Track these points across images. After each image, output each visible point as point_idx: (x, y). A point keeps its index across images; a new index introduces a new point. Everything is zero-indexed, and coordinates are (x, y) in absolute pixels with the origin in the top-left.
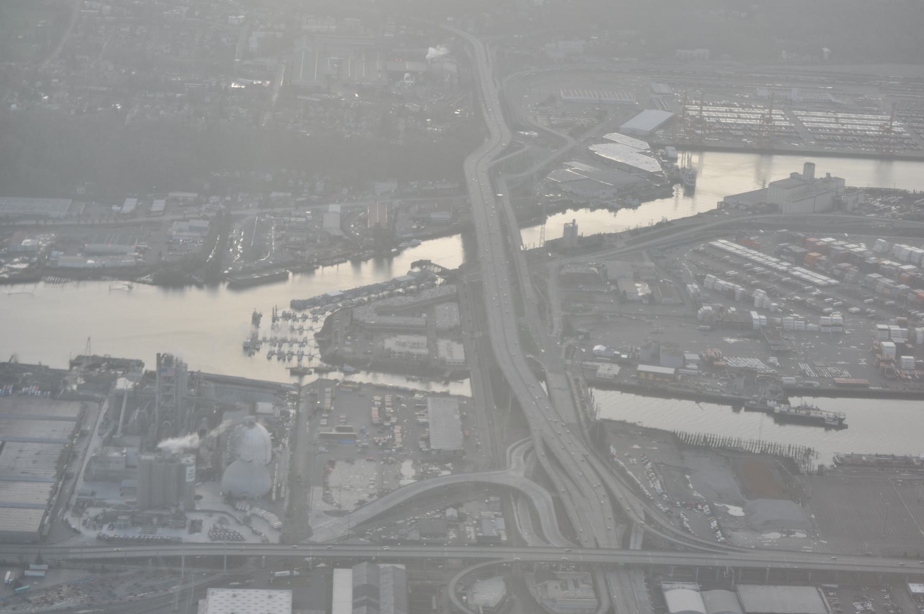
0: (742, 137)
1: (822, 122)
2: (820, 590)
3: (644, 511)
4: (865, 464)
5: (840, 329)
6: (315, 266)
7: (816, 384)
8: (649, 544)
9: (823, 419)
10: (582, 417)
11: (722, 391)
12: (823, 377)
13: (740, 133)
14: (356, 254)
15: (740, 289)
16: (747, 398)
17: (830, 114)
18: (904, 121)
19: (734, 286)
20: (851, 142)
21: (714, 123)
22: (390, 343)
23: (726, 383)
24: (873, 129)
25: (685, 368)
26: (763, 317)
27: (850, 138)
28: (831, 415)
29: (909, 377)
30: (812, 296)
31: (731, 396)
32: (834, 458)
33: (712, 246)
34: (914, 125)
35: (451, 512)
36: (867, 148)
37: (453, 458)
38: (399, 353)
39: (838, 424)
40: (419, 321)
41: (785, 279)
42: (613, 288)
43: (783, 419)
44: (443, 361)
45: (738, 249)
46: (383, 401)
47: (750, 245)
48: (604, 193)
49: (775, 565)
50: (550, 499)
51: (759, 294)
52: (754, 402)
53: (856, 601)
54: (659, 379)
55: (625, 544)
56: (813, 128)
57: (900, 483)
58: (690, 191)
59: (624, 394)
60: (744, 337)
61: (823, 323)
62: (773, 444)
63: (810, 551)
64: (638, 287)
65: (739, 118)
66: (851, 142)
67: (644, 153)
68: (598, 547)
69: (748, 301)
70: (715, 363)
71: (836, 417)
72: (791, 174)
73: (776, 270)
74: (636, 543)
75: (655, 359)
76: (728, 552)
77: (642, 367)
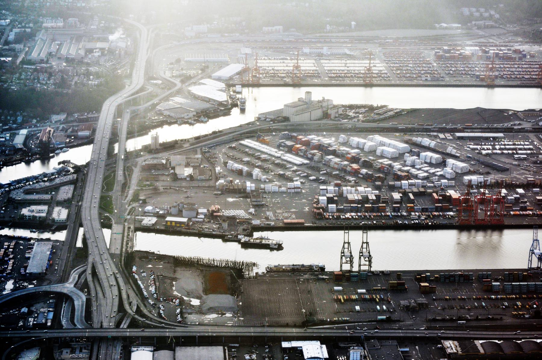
0: (285, 77)
1: (336, 66)
2: (226, 348)
3: (138, 306)
4: (284, 271)
5: (299, 190)
7: (273, 223)
8: (134, 324)
9: (269, 245)
10: (124, 250)
11: (214, 231)
12: (278, 219)
14: (27, 159)
15: (245, 169)
16: (227, 234)
17: (343, 61)
18: (387, 63)
19: (242, 168)
20: (349, 77)
21: (270, 70)
22: (25, 211)
24: (535, 70)
26: (253, 185)
27: (349, 75)
28: (274, 242)
29: (331, 217)
30: (291, 171)
31: (218, 233)
33: (241, 144)
34: (392, 65)
35: (24, 310)
36: (358, 80)
37: (40, 278)
38: (29, 216)
40: (47, 197)
41: (277, 161)
42: (172, 171)
43: (246, 246)
44: (53, 220)
45: (255, 145)
46: (9, 246)
47: (263, 142)
48: (188, 115)
49: (202, 334)
50: (85, 300)
51: (256, 172)
52: (231, 236)
53: (247, 354)
54: (178, 225)
55: (118, 325)
56: (328, 70)
57: (301, 281)
58: (243, 111)
59: (157, 235)
61: (289, 187)
62: (241, 262)
63: (231, 325)
64: (186, 171)
65: (287, 66)
66: (349, 77)
67: (221, 90)
68: (101, 327)
69: (249, 175)
70: (215, 214)
72: (299, 99)
75: (180, 214)
76: (176, 328)
77: (169, 219)
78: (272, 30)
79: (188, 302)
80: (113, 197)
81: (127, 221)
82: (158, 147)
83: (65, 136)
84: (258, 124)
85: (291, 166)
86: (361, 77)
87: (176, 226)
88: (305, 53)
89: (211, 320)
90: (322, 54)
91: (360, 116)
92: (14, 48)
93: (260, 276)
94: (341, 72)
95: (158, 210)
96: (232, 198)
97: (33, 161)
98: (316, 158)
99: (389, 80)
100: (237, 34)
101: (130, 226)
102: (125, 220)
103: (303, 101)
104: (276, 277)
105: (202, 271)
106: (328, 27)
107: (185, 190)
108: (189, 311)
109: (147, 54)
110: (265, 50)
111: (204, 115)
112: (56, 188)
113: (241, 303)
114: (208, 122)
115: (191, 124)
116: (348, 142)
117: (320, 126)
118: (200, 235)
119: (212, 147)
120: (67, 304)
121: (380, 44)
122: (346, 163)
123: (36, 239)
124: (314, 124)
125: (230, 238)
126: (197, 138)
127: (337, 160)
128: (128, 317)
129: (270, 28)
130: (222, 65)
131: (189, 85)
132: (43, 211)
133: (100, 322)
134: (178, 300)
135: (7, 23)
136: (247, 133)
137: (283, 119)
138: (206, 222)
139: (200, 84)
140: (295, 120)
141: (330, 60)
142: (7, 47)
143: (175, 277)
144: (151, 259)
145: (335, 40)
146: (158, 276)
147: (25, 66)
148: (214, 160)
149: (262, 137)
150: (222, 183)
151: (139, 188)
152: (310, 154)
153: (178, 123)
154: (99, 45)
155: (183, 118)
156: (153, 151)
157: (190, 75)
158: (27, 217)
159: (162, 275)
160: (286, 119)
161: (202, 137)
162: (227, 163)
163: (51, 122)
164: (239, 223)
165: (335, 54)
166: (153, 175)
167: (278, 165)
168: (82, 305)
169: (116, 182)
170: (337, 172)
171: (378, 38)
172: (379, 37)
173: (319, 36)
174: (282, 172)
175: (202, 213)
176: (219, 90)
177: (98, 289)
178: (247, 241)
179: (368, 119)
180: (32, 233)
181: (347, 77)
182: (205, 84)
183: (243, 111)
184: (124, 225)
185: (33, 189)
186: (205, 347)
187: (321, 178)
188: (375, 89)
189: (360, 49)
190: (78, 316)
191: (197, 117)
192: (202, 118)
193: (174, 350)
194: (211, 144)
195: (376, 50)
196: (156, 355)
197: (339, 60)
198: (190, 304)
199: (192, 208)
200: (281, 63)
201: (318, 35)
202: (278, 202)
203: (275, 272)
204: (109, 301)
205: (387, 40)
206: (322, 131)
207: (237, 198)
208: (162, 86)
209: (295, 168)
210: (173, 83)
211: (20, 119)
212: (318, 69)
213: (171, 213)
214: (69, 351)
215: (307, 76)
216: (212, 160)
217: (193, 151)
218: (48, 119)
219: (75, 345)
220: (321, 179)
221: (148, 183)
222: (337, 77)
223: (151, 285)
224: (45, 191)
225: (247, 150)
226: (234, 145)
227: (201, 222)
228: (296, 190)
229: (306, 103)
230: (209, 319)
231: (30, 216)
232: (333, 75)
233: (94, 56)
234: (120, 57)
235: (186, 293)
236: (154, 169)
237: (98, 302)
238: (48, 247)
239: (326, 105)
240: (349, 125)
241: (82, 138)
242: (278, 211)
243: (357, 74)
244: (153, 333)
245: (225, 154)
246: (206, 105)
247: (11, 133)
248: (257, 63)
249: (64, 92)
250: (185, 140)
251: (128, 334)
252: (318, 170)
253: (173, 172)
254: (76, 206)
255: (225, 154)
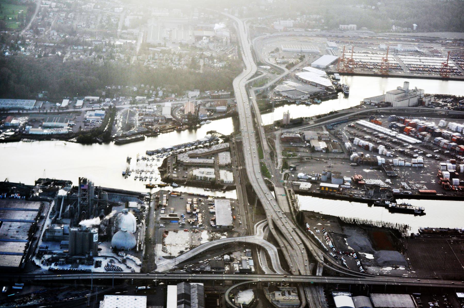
1: (413, 61)
5: (422, 165)
6: (158, 133)
7: (410, 192)
8: (326, 273)
10: (292, 209)
11: (362, 196)
13: (372, 67)
14: (179, 128)
15: (371, 145)
16: (375, 199)
17: (417, 57)
20: (427, 71)
23: (364, 192)
25: (344, 185)
27: (427, 69)
28: (417, 208)
29: (457, 189)
32: (419, 230)
33: (357, 124)
35: (226, 257)
37: (228, 230)
38: (200, 177)
39: (421, 213)
40: (211, 161)
42: (308, 144)
43: (393, 210)
44: (222, 181)
48: (303, 97)
49: (389, 283)
51: (381, 148)
52: (379, 202)
54: (331, 190)
58: (346, 95)
59: (313, 197)
60: (373, 169)
61: (413, 162)
65: (371, 59)
66: (427, 71)
69: (376, 151)
71: (420, 209)
73: (389, 135)
74: (319, 273)
75: (329, 180)
77: (322, 184)
78: (347, 27)
79: (363, 256)
80: (266, 164)
81: (285, 185)
82: (289, 123)
83: (206, 110)
84: (365, 107)
85: (407, 144)
86: (437, 72)
87: (329, 191)
88: (382, 49)
89: (388, 272)
90: (397, 50)
91: (448, 104)
92: (132, 32)
93: (416, 236)
94: (419, 66)
95: (310, 177)
96: (367, 169)
97: (184, 130)
98: (427, 139)
99: (461, 75)
100: (319, 30)
101: (290, 189)
102: (284, 184)
103: (402, 90)
104: (430, 238)
105: (365, 230)
106: (394, 27)
107: (325, 161)
108: (367, 263)
109: (249, 43)
110: (348, 44)
111: (317, 98)
112: (215, 154)
113: (408, 259)
114: (321, 104)
115: (307, 105)
116: (446, 126)
117: (418, 112)
118: (351, 199)
119: (334, 125)
120: (260, 253)
121: (443, 44)
122: (453, 144)
123: (213, 197)
124: (412, 109)
125: (378, 203)
126: (319, 117)
127: (446, 141)
128: (320, 267)
129: (346, 26)
130: (316, 56)
131: (294, 71)
132: (211, 173)
133: (297, 270)
134: (355, 254)
135: (121, 11)
136: (360, 114)
137: (386, 104)
138: (353, 189)
139: (303, 71)
140: (398, 106)
141: (405, 55)
142: (124, 31)
143: (344, 234)
144: (319, 218)
145: (403, 39)
146: (329, 233)
147: (150, 49)
148: (340, 136)
149: (375, 119)
150: (356, 156)
151: (286, 157)
152: (421, 135)
153: (297, 103)
154: (206, 33)
155: (300, 99)
156: (285, 126)
157: (292, 63)
158: (199, 178)
159: (333, 232)
160: (389, 104)
161: (323, 117)
162: (354, 139)
163: (188, 97)
164: (382, 191)
165: (407, 51)
166: (293, 147)
167: (395, 143)
168: (276, 255)
169: (264, 152)
170: (448, 151)
171: (438, 38)
172: (439, 38)
173: (389, 35)
174: (401, 149)
175: (348, 181)
176: (322, 77)
177: (285, 241)
178: (394, 207)
179: (456, 108)
180: (206, 192)
181: (425, 71)
182: (309, 71)
183: (346, 95)
184: (284, 188)
185: (195, 154)
186: (394, 295)
187: (436, 155)
188: (450, 82)
189: (427, 47)
190: (274, 263)
191: (311, 99)
192: (316, 100)
193: (369, 296)
194: (336, 122)
195: (442, 49)
196: (356, 300)
197: (412, 56)
198: (366, 258)
199: (339, 176)
200: (365, 56)
201: (388, 34)
202: (407, 174)
203: (427, 233)
204: (299, 252)
205: (447, 41)
206: (423, 115)
207: (371, 169)
208: (271, 71)
209: (411, 146)
210: (281, 69)
211: (161, 93)
212: (398, 63)
213: (321, 179)
214: (280, 293)
215: (391, 68)
216: (339, 136)
217: (319, 128)
218: (184, 94)
219: (283, 288)
220: (436, 157)
221: (291, 153)
222: (416, 70)
223: (327, 240)
224: (207, 156)
225: (365, 129)
226: (352, 124)
227: (349, 188)
228: (419, 165)
229: (405, 92)
230: (387, 271)
231: (202, 177)
232: (413, 69)
233: (203, 42)
234: (227, 44)
235: (359, 248)
236: (293, 142)
237: (289, 253)
238: (227, 205)
239: (419, 94)
240: (443, 112)
241: (220, 112)
242: (411, 182)
243: (433, 68)
244: (352, 281)
245: (346, 131)
246: (317, 89)
247: (157, 105)
248: (344, 55)
249: (197, 72)
250: (309, 118)
251: (327, 281)
252: (431, 149)
253: (309, 145)
254: (237, 170)
255: (346, 131)
